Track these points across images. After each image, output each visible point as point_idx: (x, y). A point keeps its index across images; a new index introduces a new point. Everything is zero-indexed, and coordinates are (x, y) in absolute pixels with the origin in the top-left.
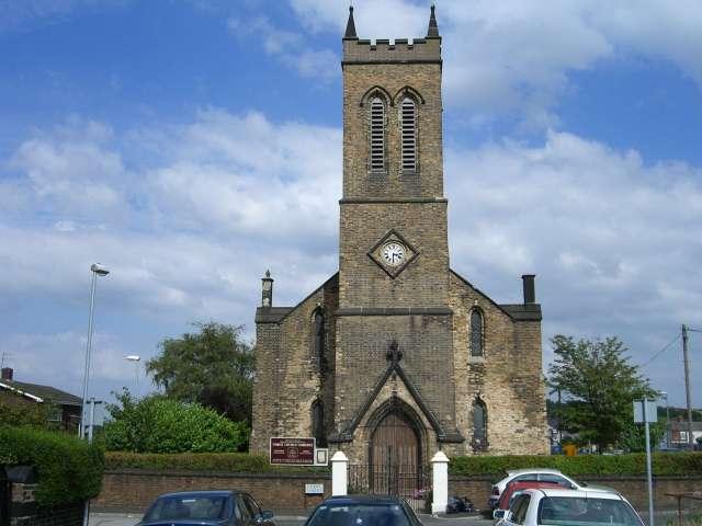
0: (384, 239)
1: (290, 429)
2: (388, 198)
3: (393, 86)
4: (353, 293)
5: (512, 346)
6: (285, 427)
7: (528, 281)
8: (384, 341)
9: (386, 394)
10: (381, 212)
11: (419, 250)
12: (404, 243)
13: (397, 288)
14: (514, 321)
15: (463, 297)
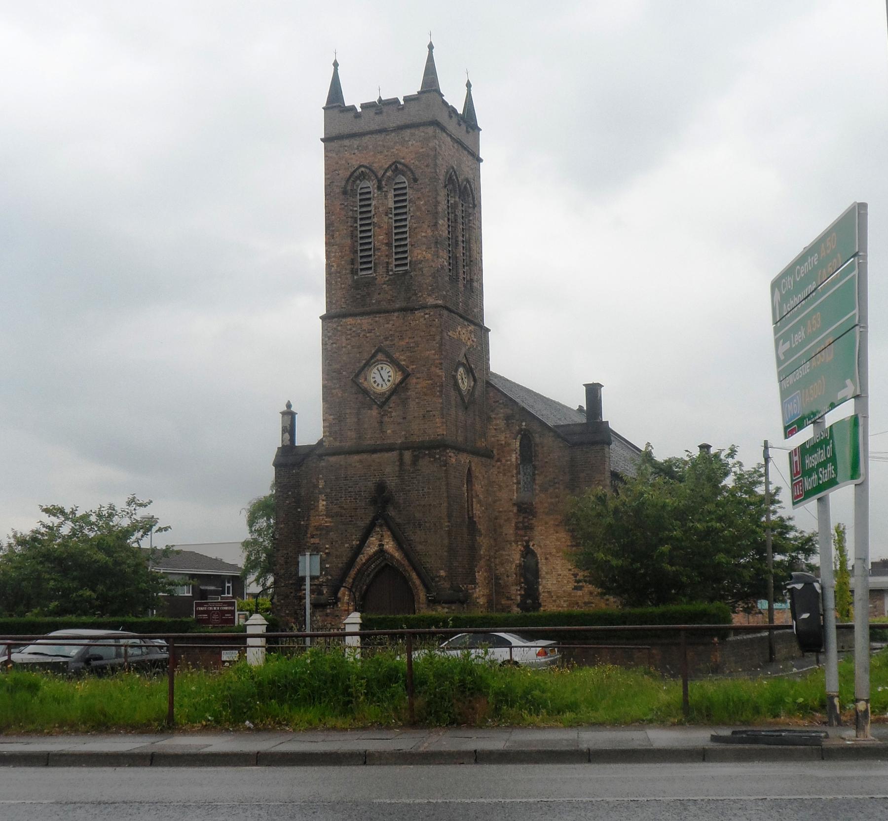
4: (337, 428)
9: (371, 548)
10: (365, 327)
11: (409, 370)
13: (386, 419)
15: (508, 418)
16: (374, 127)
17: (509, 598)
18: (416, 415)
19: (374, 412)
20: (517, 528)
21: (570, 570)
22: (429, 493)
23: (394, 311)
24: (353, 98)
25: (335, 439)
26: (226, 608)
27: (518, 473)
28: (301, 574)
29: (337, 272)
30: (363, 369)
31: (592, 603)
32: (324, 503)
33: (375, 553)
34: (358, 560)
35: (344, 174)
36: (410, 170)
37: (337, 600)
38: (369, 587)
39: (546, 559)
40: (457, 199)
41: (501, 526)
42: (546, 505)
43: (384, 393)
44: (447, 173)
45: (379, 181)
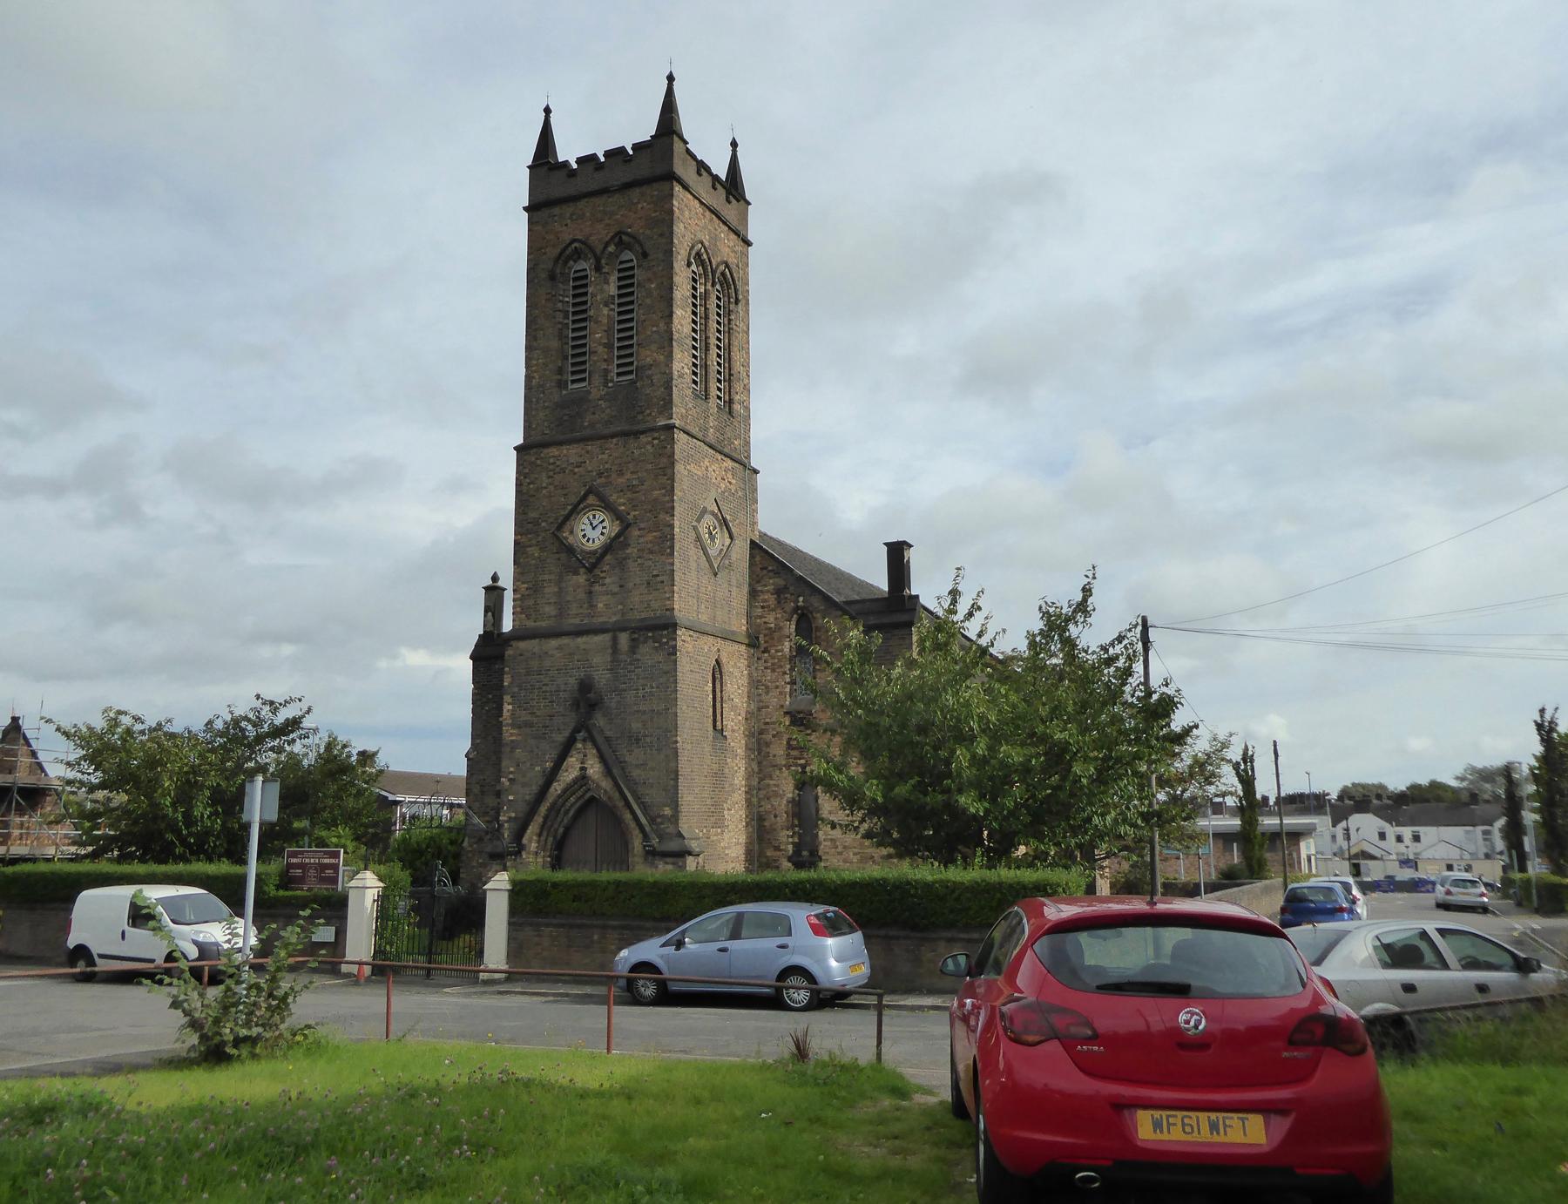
0: (576, 507)
2: (588, 432)
3: (599, 234)
7: (897, 554)
8: (572, 681)
9: (569, 773)
12: (608, 507)
13: (597, 588)
15: (779, 592)
16: (594, 187)
17: (777, 849)
18: (638, 581)
19: (581, 579)
20: (790, 747)
22: (651, 694)
23: (613, 436)
24: (568, 151)
25: (528, 616)
26: (327, 861)
27: (792, 669)
28: (245, 818)
29: (540, 386)
30: (567, 518)
33: (576, 781)
34: (552, 790)
35: (553, 252)
36: (639, 242)
37: (520, 849)
38: (567, 829)
40: (709, 287)
41: (768, 745)
43: (595, 552)
44: (692, 248)
45: (598, 260)
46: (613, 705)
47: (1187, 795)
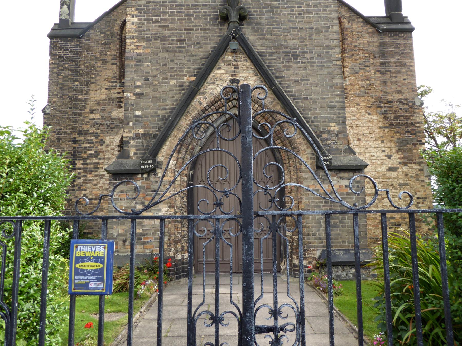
1: (91, 171)
5: (378, 62)
6: (85, 169)
9: (218, 82)
14: (379, 32)
21: (383, 151)
31: (407, 184)
32: (136, 20)
34: (195, 102)
39: (359, 140)
42: (357, 87)
46: (264, 21)
47: (33, 338)
